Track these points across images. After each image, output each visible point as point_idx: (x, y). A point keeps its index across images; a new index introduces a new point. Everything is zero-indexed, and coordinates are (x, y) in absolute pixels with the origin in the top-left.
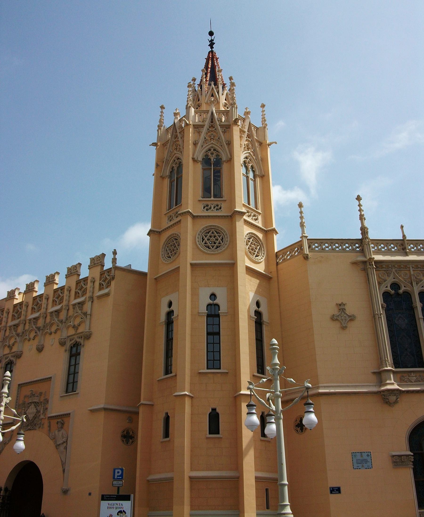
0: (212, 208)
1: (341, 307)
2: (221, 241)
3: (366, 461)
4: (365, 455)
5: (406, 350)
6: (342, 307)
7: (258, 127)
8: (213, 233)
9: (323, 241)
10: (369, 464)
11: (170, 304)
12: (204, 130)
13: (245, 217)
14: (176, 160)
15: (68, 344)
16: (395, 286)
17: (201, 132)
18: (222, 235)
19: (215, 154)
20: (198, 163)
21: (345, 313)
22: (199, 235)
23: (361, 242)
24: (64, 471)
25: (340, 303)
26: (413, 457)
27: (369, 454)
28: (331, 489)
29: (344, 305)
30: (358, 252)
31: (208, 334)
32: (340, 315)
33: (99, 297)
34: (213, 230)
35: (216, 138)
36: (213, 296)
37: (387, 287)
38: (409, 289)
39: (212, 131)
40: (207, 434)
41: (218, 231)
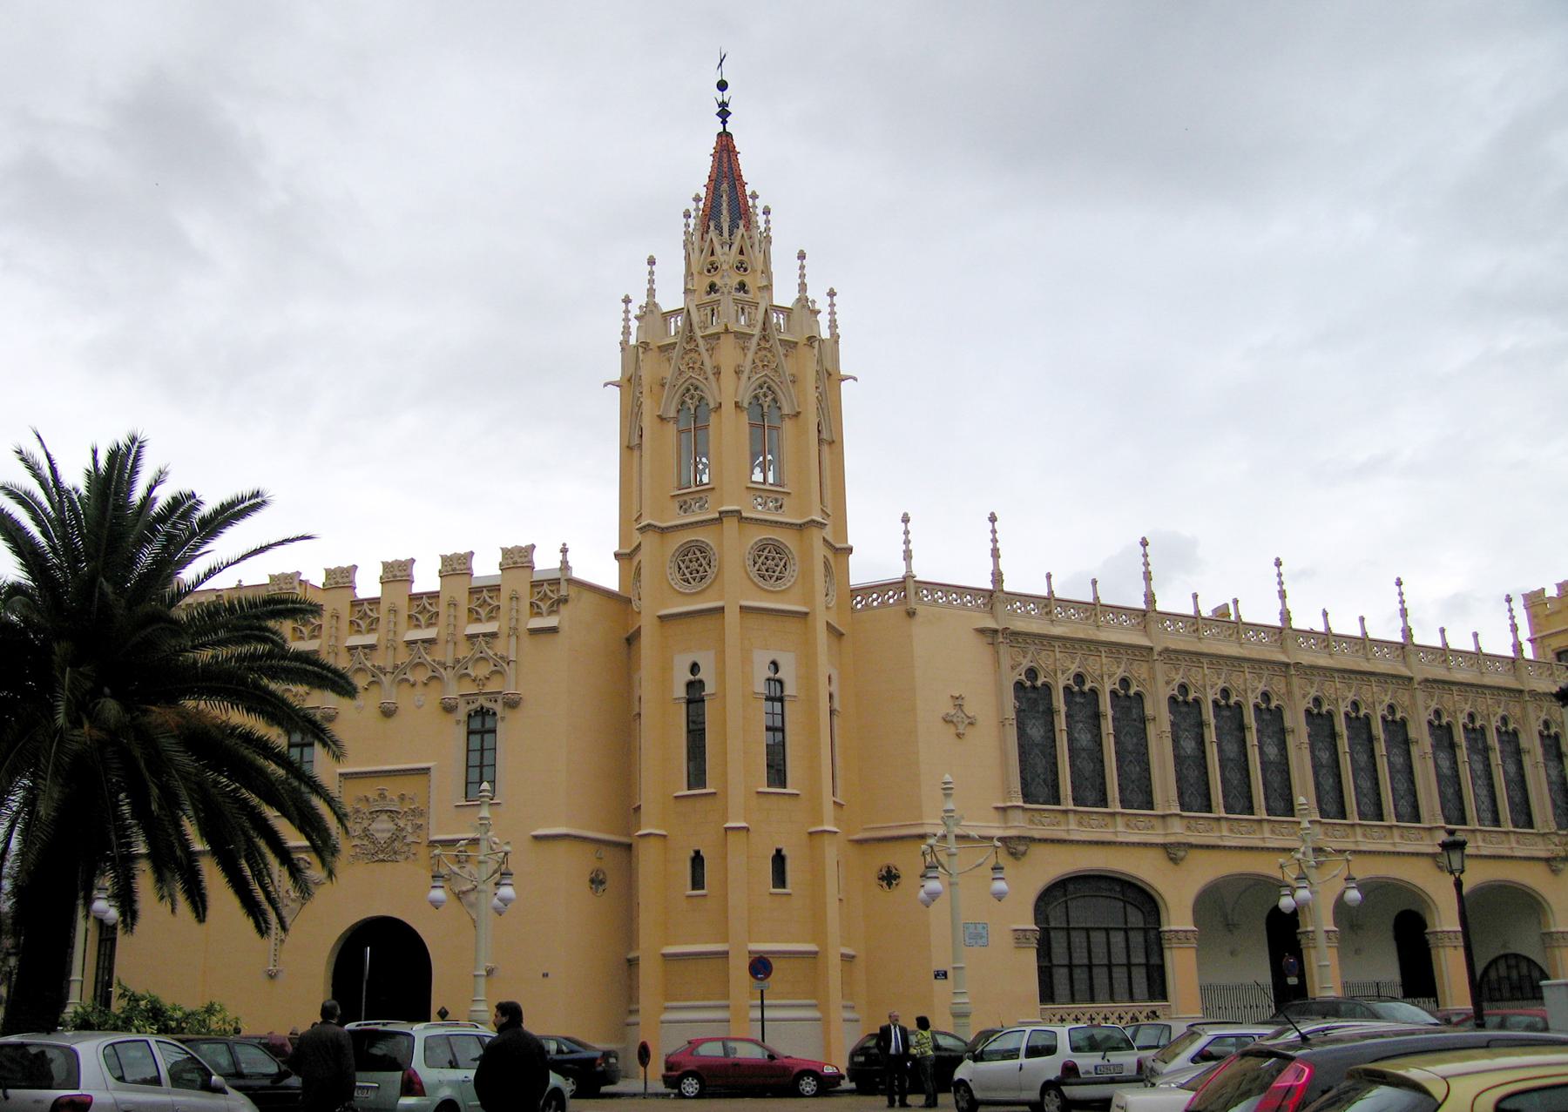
1: (958, 702)
2: (774, 578)
4: (980, 927)
6: (959, 702)
8: (769, 552)
9: (936, 587)
10: (984, 940)
11: (695, 668)
14: (692, 391)
15: (462, 714)
16: (1032, 673)
17: (748, 349)
18: (786, 558)
21: (962, 711)
22: (750, 553)
25: (957, 695)
29: (962, 699)
36: (775, 665)
37: (1020, 675)
39: (765, 349)
41: (779, 549)
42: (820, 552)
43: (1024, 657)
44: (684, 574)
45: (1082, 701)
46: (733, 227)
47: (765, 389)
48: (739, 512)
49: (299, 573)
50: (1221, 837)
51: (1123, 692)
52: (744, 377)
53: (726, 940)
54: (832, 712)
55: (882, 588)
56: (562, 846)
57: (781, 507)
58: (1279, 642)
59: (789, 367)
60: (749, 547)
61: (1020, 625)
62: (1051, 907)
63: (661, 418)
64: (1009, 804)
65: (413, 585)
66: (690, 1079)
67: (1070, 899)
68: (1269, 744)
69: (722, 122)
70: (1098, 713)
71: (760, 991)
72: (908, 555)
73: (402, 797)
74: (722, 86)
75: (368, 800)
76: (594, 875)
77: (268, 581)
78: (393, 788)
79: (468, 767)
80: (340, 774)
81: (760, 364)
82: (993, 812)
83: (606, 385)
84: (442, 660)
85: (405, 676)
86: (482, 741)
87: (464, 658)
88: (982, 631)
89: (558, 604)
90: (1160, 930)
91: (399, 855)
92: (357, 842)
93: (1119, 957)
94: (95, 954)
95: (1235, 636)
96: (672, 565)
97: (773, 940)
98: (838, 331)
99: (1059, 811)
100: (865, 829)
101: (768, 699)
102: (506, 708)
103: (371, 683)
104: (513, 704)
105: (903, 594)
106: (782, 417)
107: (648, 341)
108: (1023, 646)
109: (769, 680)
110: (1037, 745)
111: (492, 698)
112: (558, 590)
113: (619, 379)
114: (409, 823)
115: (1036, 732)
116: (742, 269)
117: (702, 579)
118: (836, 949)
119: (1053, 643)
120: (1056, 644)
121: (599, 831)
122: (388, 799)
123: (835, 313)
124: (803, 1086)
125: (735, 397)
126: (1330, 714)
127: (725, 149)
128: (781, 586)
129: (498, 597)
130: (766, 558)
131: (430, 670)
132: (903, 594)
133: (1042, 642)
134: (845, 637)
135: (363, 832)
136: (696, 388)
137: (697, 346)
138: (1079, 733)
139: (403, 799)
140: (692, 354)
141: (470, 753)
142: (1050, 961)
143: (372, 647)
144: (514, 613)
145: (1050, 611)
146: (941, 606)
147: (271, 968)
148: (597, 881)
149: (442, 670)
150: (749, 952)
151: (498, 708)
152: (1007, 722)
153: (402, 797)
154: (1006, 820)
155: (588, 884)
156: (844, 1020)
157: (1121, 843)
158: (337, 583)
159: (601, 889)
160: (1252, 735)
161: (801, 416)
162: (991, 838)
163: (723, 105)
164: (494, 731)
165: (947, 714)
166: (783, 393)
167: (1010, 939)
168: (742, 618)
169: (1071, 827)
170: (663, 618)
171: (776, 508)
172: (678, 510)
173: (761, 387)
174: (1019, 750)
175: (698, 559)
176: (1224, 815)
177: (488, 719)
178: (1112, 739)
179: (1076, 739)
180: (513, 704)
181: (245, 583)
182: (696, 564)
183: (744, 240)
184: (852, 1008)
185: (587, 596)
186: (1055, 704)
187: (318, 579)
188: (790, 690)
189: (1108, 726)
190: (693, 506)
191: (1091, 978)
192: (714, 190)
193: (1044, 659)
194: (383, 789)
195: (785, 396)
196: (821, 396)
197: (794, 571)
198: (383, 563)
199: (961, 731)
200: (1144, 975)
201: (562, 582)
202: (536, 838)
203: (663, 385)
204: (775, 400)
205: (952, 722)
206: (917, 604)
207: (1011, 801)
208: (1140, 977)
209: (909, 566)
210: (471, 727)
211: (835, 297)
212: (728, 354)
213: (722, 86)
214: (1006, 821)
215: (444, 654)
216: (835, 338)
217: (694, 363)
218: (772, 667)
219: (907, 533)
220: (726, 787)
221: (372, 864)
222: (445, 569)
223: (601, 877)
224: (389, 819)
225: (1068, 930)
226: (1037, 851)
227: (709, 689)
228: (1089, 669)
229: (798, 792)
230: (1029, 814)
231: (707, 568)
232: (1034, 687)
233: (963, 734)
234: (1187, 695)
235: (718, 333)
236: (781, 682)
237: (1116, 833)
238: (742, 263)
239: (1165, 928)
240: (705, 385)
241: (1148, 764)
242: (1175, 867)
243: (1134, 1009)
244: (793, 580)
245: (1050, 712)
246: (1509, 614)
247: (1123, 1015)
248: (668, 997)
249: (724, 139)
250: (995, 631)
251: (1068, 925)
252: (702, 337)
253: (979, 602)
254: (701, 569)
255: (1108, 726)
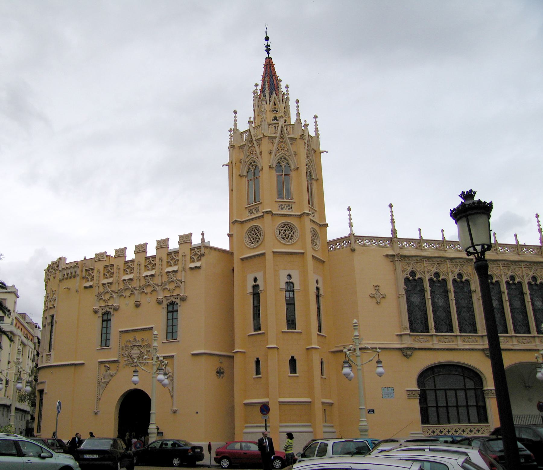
0: (285, 206)
2: (289, 239)
3: (390, 393)
4: (390, 389)
5: (418, 320)
7: (312, 136)
8: (286, 228)
11: (255, 280)
12: (277, 141)
13: (311, 217)
14: (253, 163)
15: (100, 314)
16: (413, 273)
17: (274, 143)
19: (285, 162)
20: (273, 169)
22: (277, 229)
23: (390, 239)
24: (172, 397)
26: (419, 392)
27: (392, 389)
28: (369, 410)
30: (388, 247)
31: (286, 304)
32: (375, 293)
33: (192, 269)
34: (287, 225)
35: (285, 148)
36: (290, 276)
37: (407, 275)
38: (422, 277)
39: (282, 142)
40: (288, 374)
41: (290, 226)
42: (309, 226)
43: (409, 266)
44: (251, 240)
45: (439, 285)
46: (271, 94)
47: (283, 159)
48: (270, 211)
49: (106, 252)
50: (513, 345)
51: (459, 280)
52: (273, 155)
53: (267, 396)
54: (318, 296)
55: (340, 240)
56: (203, 358)
57: (291, 208)
58: (540, 252)
59: (292, 149)
60: (277, 225)
61: (406, 252)
62: (426, 380)
63: (241, 176)
64: (403, 333)
65: (147, 253)
66: (225, 460)
67: (436, 376)
68: (537, 301)
69: (267, 53)
70: (447, 290)
71: (265, 420)
72: (351, 225)
73: (143, 340)
74: (267, 39)
75: (130, 341)
76: (218, 370)
77: (94, 256)
78: (138, 336)
79: (167, 326)
80: (120, 331)
81: (280, 149)
82: (396, 338)
83: (223, 166)
84: (157, 283)
85: (143, 290)
86: (173, 315)
87: (165, 281)
88: (387, 256)
89: (201, 257)
90: (483, 389)
91: (141, 363)
92: (126, 359)
93: (462, 402)
94: (39, 405)
95: (516, 251)
96: (246, 237)
97: (290, 397)
98: (319, 132)
99: (531, 337)
100: (336, 347)
101: (286, 291)
102: (181, 301)
103: (131, 294)
104: (184, 299)
105: (349, 242)
106: (291, 170)
107: (234, 145)
108: (529, 267)
109: (287, 283)
110: (417, 306)
111: (176, 297)
112: (201, 251)
113: (228, 163)
114: (145, 350)
115: (416, 300)
116: (275, 111)
117: (258, 241)
118: (320, 399)
119: (521, 264)
120: (424, 260)
121: (222, 351)
122: (137, 341)
123: (317, 125)
124: (275, 464)
125: (269, 163)
126: (520, 283)
127: (269, 64)
128: (292, 242)
129: (178, 256)
130: (285, 231)
131: (152, 287)
132: (349, 242)
133: (445, 261)
134: (326, 263)
135: (129, 354)
136: (254, 162)
137: (254, 144)
138: (438, 299)
139: (143, 341)
140: (252, 148)
141: (168, 320)
142: (427, 404)
143: (131, 280)
144: (184, 261)
145: (421, 245)
146: (368, 246)
147: (95, 410)
148: (220, 372)
149: (157, 287)
150: (279, 402)
151: (178, 301)
152: (400, 296)
153: (143, 340)
154: (402, 340)
155: (214, 373)
156: (323, 432)
157: (460, 349)
158: (184, 241)
159: (222, 376)
160: (505, 296)
161: (299, 168)
162: (376, 348)
163: (268, 47)
164: (177, 311)
165: (372, 294)
166: (291, 160)
167: (405, 395)
168: (274, 256)
169: (434, 343)
170: (242, 259)
171: (289, 209)
172: (248, 213)
173: (281, 158)
174: (408, 308)
175: (256, 233)
176: (514, 334)
177: (175, 306)
178: (454, 301)
179: (436, 302)
180: (184, 299)
181: (87, 258)
182: (255, 236)
183: (276, 99)
184: (332, 426)
185: (214, 254)
186: (449, 287)
187: (112, 254)
188: (296, 287)
189: (452, 296)
190: (254, 211)
191: (448, 413)
192: (273, 81)
193: (465, 269)
194: (135, 337)
195: (292, 161)
196: (311, 160)
197: (298, 235)
198: (135, 245)
199: (378, 301)
200: (476, 411)
201: (202, 247)
202: (193, 355)
203: (241, 162)
204: (287, 163)
205: (374, 297)
206: (355, 246)
207: (404, 332)
208: (473, 412)
209: (351, 229)
210: (169, 310)
211: (317, 119)
212: (266, 146)
213: (267, 39)
214: (402, 341)
215: (158, 280)
216: (318, 136)
217: (253, 151)
218: (289, 277)
219: (350, 215)
220: (267, 330)
221: (131, 367)
222: (158, 246)
223: (222, 370)
224: (138, 349)
225: (435, 390)
226: (417, 354)
227: (261, 288)
228: (441, 270)
229: (301, 331)
230: (413, 337)
231: (260, 236)
232: (414, 280)
233: (380, 302)
234: (537, 281)
235: (261, 138)
236: (293, 283)
237: (536, 345)
238: (275, 109)
239: (485, 388)
240: (257, 160)
241: (473, 312)
242: (407, 359)
243: (449, 427)
244: (297, 239)
245: (423, 291)
246: (390, 213)
247: (472, 429)
248: (246, 422)
249: (268, 60)
250: (393, 256)
251: (435, 387)
252: (255, 140)
253: (437, 246)
254: (257, 237)
255: (452, 296)
